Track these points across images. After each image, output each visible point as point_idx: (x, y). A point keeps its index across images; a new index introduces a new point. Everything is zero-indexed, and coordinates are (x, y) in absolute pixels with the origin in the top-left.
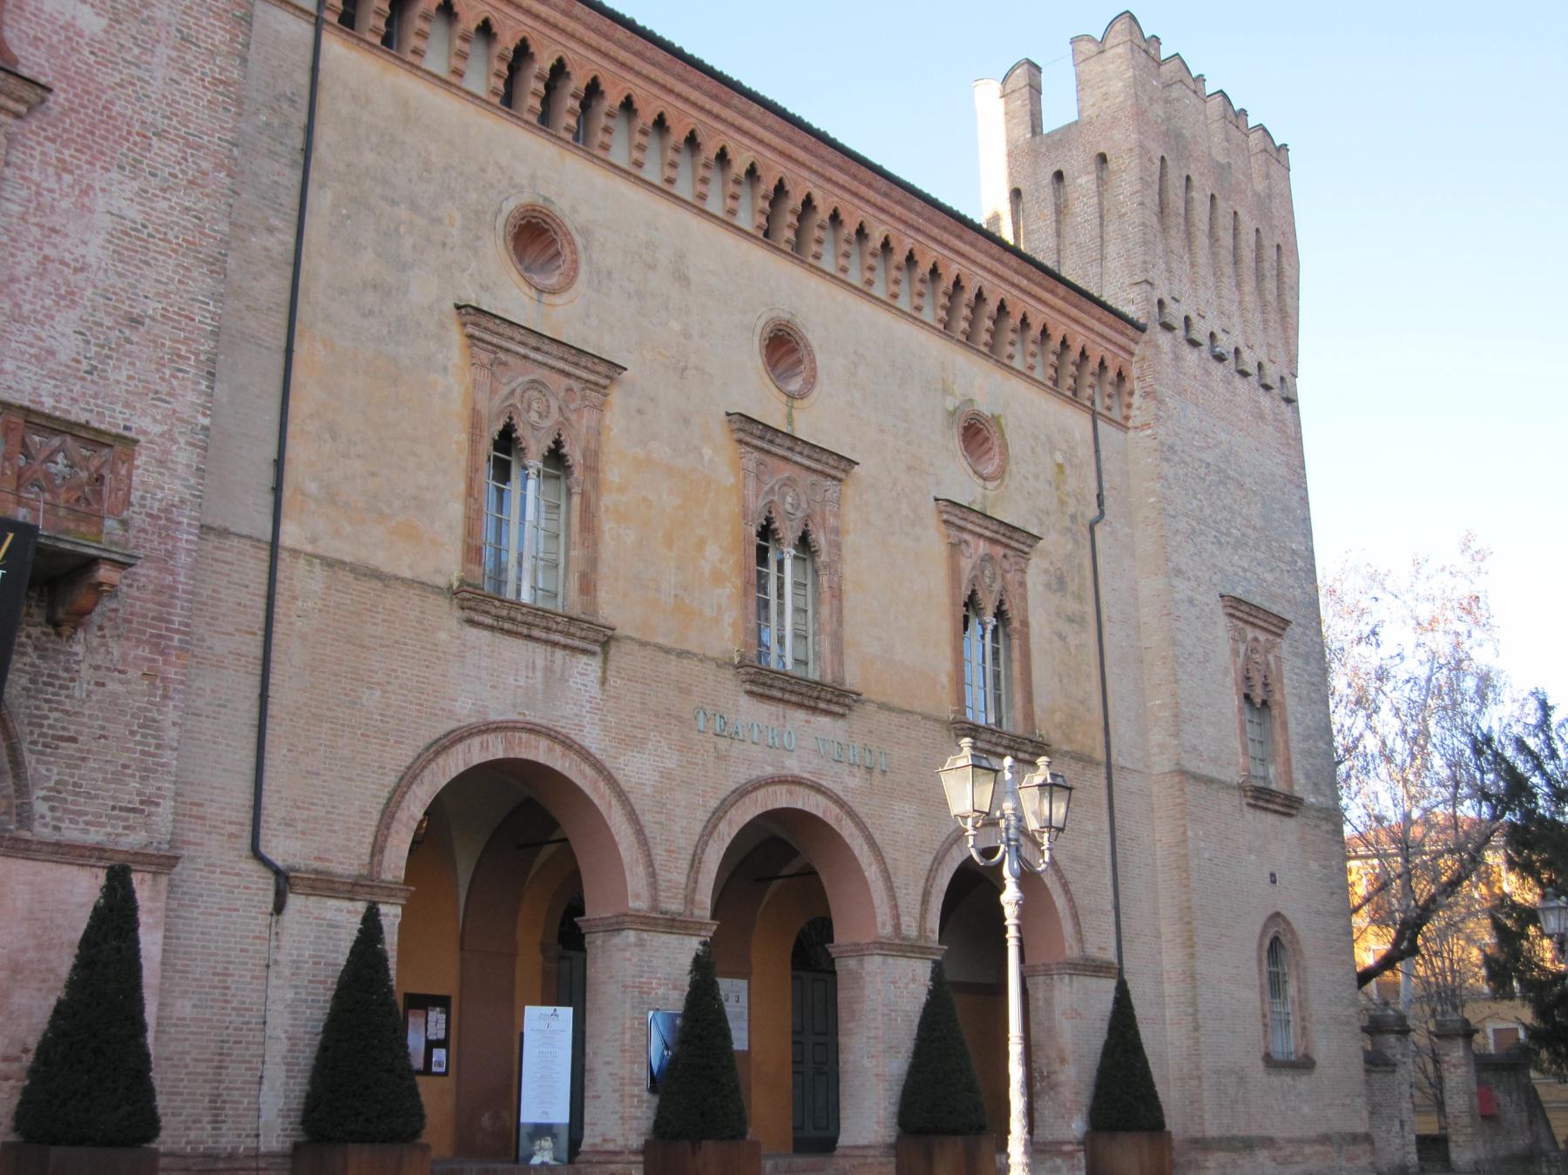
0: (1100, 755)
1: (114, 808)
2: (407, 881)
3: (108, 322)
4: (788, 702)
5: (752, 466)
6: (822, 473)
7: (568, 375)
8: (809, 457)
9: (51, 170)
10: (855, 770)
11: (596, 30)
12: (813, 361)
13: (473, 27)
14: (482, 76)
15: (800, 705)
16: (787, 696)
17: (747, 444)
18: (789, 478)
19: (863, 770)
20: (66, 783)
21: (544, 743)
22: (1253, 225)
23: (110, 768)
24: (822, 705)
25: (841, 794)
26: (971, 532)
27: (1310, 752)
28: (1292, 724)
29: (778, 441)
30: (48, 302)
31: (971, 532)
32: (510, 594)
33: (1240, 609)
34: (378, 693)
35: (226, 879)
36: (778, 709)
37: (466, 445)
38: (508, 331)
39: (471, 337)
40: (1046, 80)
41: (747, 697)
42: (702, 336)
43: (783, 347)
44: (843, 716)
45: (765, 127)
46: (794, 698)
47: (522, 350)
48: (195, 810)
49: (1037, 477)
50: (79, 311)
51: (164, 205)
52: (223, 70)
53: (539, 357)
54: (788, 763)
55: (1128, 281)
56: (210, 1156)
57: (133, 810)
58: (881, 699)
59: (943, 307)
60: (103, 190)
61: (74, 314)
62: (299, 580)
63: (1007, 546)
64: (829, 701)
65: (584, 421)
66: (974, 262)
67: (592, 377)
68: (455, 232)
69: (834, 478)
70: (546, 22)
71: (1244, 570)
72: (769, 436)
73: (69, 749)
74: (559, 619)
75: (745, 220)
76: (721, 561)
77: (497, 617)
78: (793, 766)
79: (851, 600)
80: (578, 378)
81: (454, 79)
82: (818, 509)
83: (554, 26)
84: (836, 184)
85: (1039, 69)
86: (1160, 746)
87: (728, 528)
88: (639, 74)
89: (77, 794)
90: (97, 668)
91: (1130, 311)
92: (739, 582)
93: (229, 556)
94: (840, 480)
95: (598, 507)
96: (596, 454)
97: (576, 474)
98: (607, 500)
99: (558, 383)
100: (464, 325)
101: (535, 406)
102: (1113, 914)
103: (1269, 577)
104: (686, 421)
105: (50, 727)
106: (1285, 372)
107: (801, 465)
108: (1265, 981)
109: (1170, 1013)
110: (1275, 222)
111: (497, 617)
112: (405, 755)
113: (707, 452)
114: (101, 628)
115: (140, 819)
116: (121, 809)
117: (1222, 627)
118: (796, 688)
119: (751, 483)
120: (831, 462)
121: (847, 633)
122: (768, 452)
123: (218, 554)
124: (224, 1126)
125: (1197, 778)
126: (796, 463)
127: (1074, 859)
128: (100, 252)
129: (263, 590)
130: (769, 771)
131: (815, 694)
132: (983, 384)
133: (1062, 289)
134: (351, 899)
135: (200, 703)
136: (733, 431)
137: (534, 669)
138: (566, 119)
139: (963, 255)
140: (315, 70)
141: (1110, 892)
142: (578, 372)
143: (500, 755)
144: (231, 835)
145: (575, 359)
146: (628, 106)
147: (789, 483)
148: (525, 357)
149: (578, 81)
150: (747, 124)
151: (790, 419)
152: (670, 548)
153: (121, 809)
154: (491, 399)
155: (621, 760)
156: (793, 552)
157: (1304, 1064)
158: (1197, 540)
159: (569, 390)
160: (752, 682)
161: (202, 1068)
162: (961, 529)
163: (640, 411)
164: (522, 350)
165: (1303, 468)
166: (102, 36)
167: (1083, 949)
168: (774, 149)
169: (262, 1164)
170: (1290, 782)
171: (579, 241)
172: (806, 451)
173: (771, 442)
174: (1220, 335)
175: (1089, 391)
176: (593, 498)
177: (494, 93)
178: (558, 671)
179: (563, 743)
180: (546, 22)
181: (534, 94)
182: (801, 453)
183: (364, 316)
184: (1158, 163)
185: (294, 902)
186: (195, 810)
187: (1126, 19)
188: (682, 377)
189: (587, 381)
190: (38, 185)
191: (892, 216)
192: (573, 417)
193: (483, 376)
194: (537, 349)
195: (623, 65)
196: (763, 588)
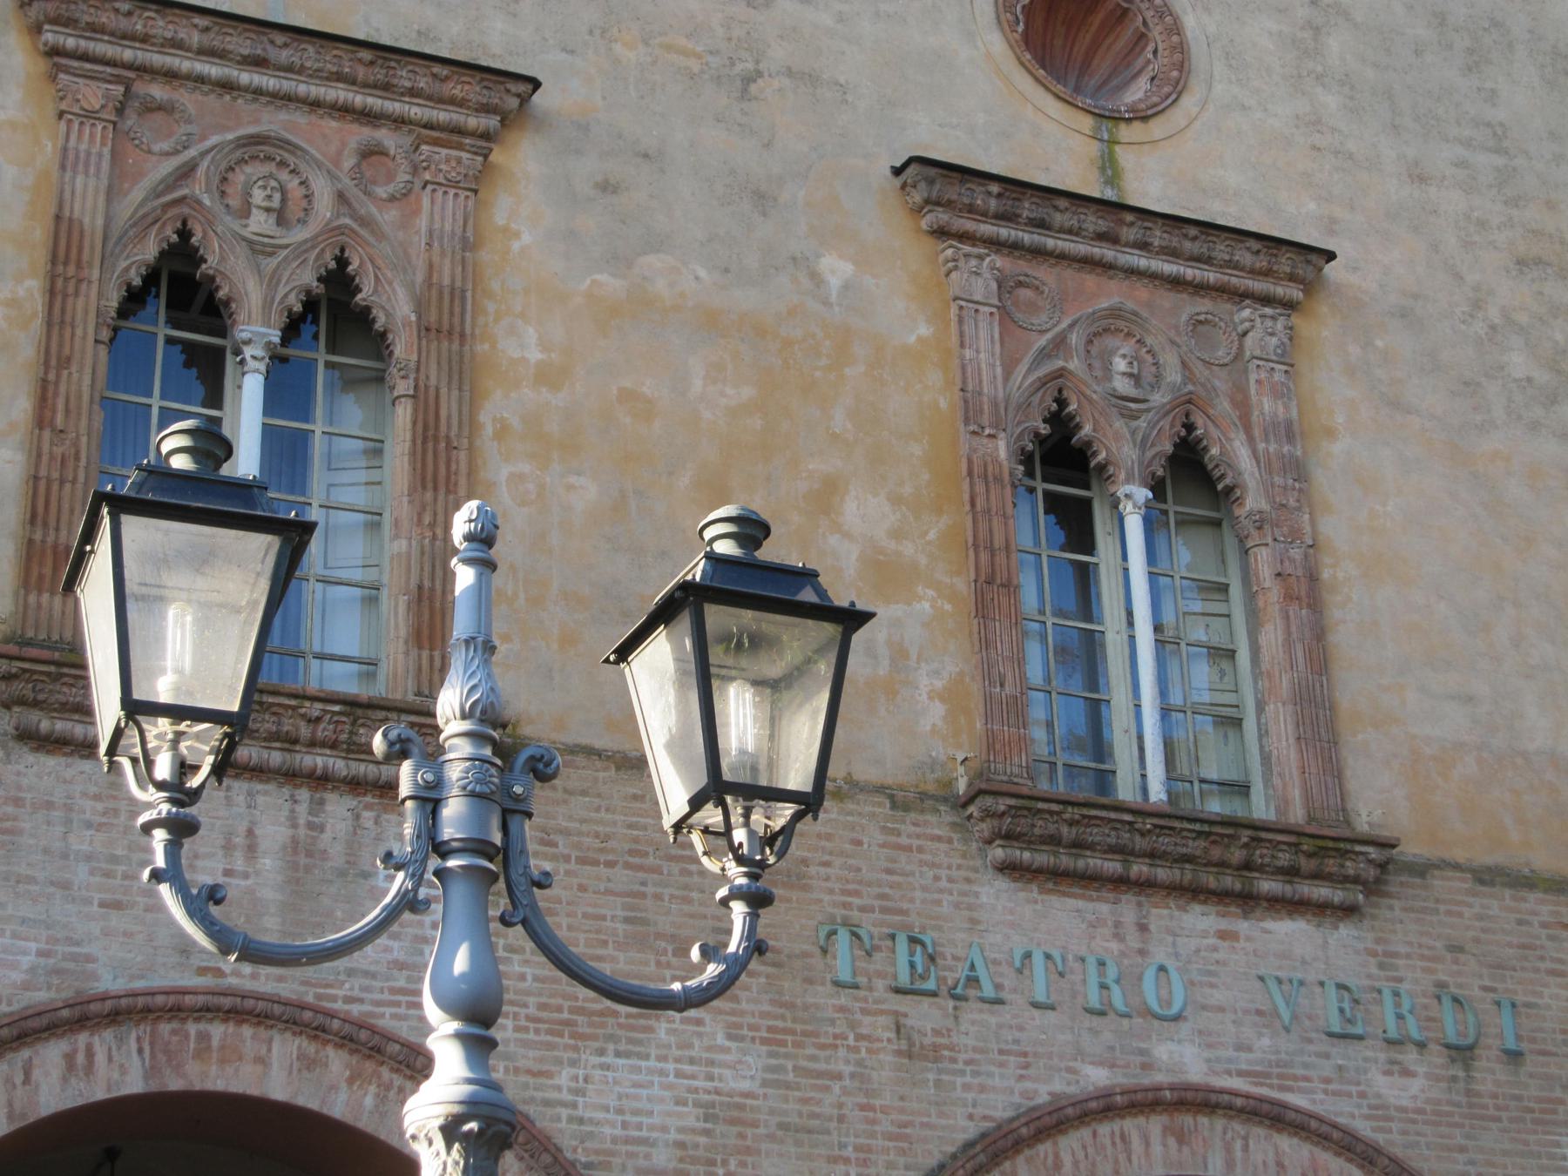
4: (1145, 886)
5: (983, 288)
6: (1221, 290)
7: (367, 117)
8: (1173, 253)
10: (1410, 1056)
12: (1176, 29)
15: (1194, 893)
16: (1139, 869)
17: (964, 237)
18: (1115, 313)
19: (1437, 1056)
21: (284, 1047)
24: (1267, 886)
25: (1364, 1128)
29: (1129, 234)
32: (1125, 791)
36: (1128, 908)
37: (38, 303)
39: (54, 52)
41: (1003, 883)
44: (1349, 911)
47: (213, 70)
53: (269, 82)
54: (1162, 1052)
64: (1291, 873)
65: (422, 223)
67: (442, 116)
69: (1266, 300)
72: (1027, 209)
74: (316, 709)
76: (897, 534)
78: (1183, 1059)
79: (1354, 606)
80: (400, 122)
82: (1221, 382)
87: (917, 450)
92: (963, 585)
94: (1290, 306)
95: (471, 425)
96: (457, 295)
97: (399, 350)
98: (499, 407)
99: (338, 141)
100: (37, 29)
101: (258, 196)
104: (762, 200)
107: (1154, 276)
113: (836, 269)
118: (1164, 843)
119: (986, 333)
120: (1245, 258)
121: (1352, 689)
122: (1038, 253)
126: (1132, 272)
130: (1097, 1077)
131: (1237, 855)
136: (918, 211)
137: (251, 849)
142: (394, 107)
143: (134, 1084)
145: (379, 74)
148: (227, 86)
151: (1109, 168)
154: (1007, 375)
155: (564, 1078)
159: (371, 152)
160: (1009, 837)
163: (607, 187)
164: (213, 70)
172: (1158, 237)
173: (1041, 225)
176: (449, 405)
178: (337, 852)
179: (347, 1041)
182: (1143, 246)
188: (744, 95)
189: (429, 126)
192: (388, 217)
193: (94, 141)
194: (259, 63)
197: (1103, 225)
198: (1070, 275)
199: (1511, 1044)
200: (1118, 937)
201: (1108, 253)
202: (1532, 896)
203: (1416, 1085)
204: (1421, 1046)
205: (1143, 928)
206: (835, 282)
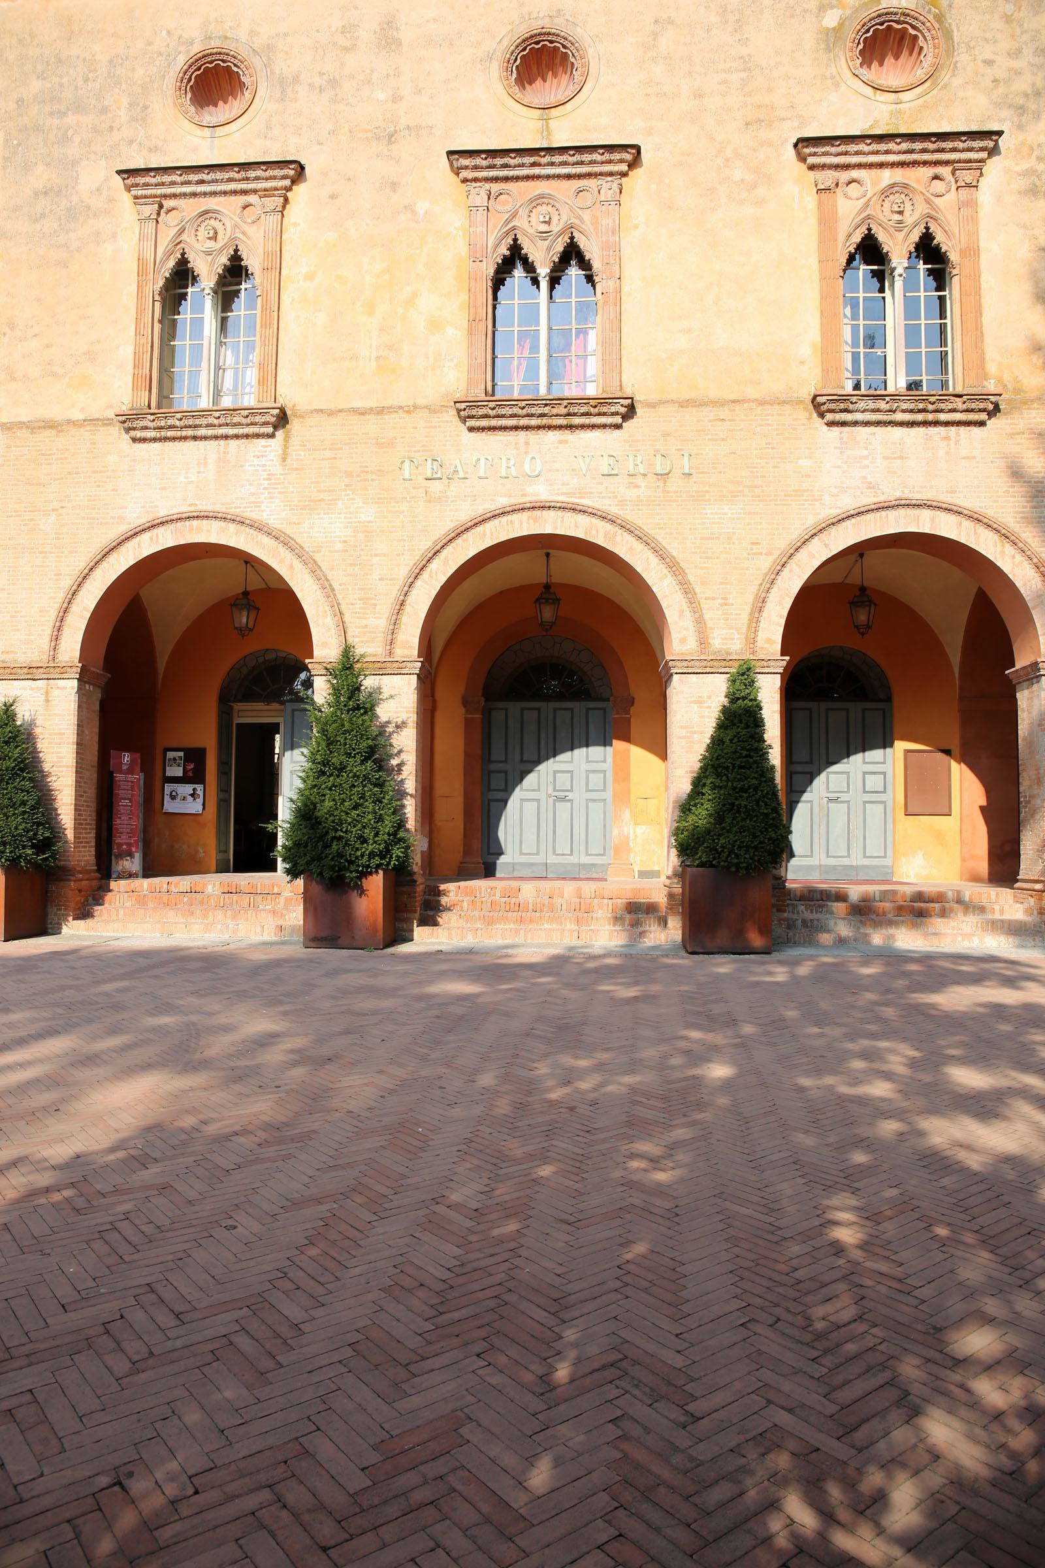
4: (527, 428)
10: (639, 480)
26: (860, 166)
29: (544, 160)
31: (860, 166)
34: (53, 518)
46: (534, 422)
54: (530, 490)
78: (541, 492)
80: (255, 191)
109: (803, 970)
112: (81, 562)
117: (118, 178)
120: (598, 158)
122: (506, 179)
126: (548, 177)
145: (243, 174)
152: (371, 314)
173: (506, 166)
183: (36, 220)
197: (532, 160)
198: (522, 184)
199: (687, 471)
200: (517, 448)
201: (536, 171)
202: (705, 410)
203: (639, 492)
204: (645, 475)
205: (527, 443)
206: (422, 212)
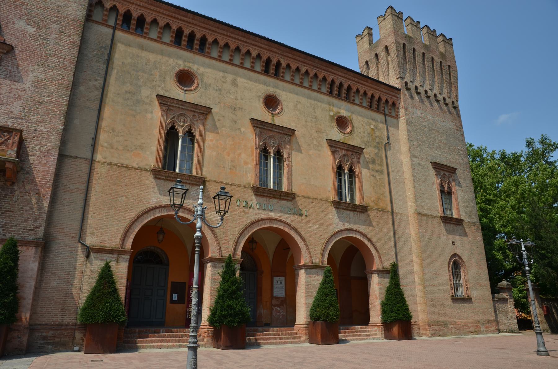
0: (389, 209)
1: (24, 229)
2: (131, 249)
3: (31, 104)
9: (15, 67)
11: (203, 23)
13: (285, 66)
14: (167, 38)
20: (8, 223)
22: (439, 60)
23: (24, 219)
25: (290, 222)
27: (467, 206)
28: (460, 199)
30: (12, 99)
33: (437, 166)
35: (70, 249)
38: (172, 101)
40: (374, 32)
42: (242, 99)
43: (271, 102)
45: (262, 44)
47: (177, 106)
48: (61, 231)
49: (364, 132)
50: (22, 101)
51: (51, 73)
52: (73, 39)
55: (396, 78)
56: (60, 325)
57: (31, 230)
58: (305, 195)
59: (368, 102)
60: (32, 71)
61: (20, 102)
62: (98, 169)
63: (353, 151)
66: (338, 75)
68: (157, 77)
70: (187, 22)
71: (440, 155)
73: (11, 214)
75: (365, 104)
77: (165, 177)
80: (197, 112)
81: (159, 39)
83: (190, 23)
84: (288, 57)
85: (371, 29)
86: (411, 206)
88: (218, 33)
89: (12, 226)
90: (21, 192)
91: (396, 86)
93: (77, 163)
102: (395, 255)
103: (449, 157)
105: (4, 208)
106: (454, 100)
108: (451, 273)
109: (417, 284)
110: (447, 59)
111: (165, 177)
114: (23, 182)
115: (33, 232)
116: (27, 230)
123: (73, 163)
124: (65, 317)
125: (423, 215)
127: (380, 239)
128: (30, 86)
129: (88, 171)
132: (343, 109)
133: (370, 81)
134: (112, 254)
135: (64, 202)
138: (272, 71)
139: (334, 73)
140: (112, 40)
141: (394, 249)
144: (73, 237)
146: (387, 101)
147: (270, 137)
148: (179, 108)
149: (337, 83)
150: (256, 43)
152: (229, 156)
153: (27, 230)
156: (273, 155)
157: (468, 300)
158: (422, 147)
161: (59, 300)
162: (336, 147)
164: (177, 106)
165: (462, 126)
166: (34, 33)
167: (383, 265)
168: (266, 49)
169: (76, 328)
170: (459, 215)
171: (199, 77)
174: (447, 98)
175: (382, 108)
177: (328, 91)
180: (187, 22)
181: (184, 41)
183: (125, 100)
184: (402, 45)
185: (92, 255)
186: (61, 231)
187: (409, 19)
190: (10, 70)
191: (308, 64)
195: (213, 31)
196: (341, 182)
